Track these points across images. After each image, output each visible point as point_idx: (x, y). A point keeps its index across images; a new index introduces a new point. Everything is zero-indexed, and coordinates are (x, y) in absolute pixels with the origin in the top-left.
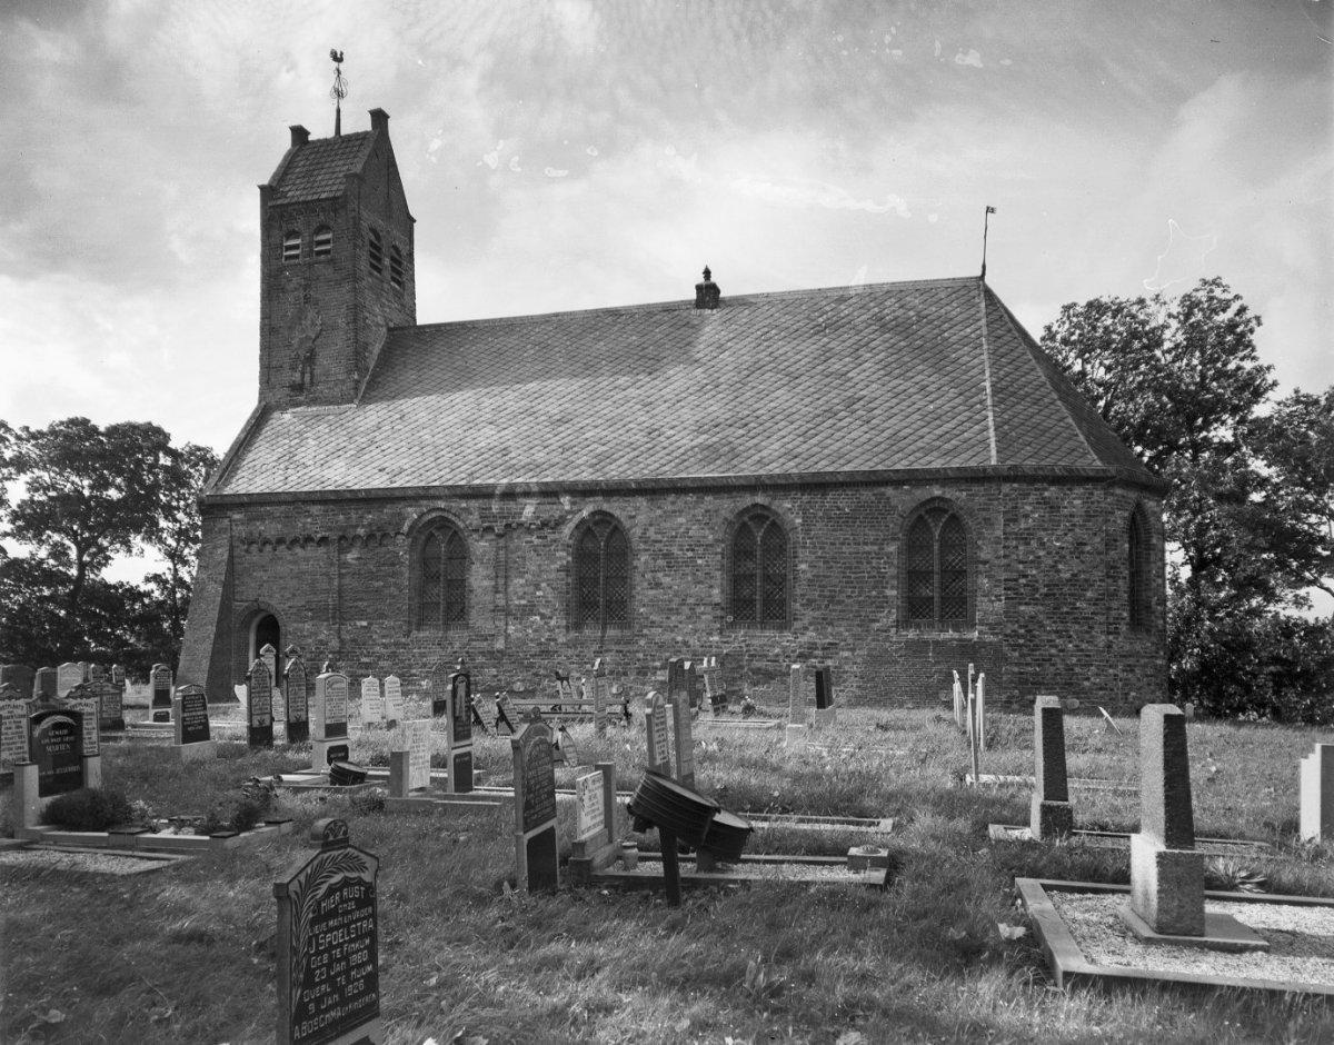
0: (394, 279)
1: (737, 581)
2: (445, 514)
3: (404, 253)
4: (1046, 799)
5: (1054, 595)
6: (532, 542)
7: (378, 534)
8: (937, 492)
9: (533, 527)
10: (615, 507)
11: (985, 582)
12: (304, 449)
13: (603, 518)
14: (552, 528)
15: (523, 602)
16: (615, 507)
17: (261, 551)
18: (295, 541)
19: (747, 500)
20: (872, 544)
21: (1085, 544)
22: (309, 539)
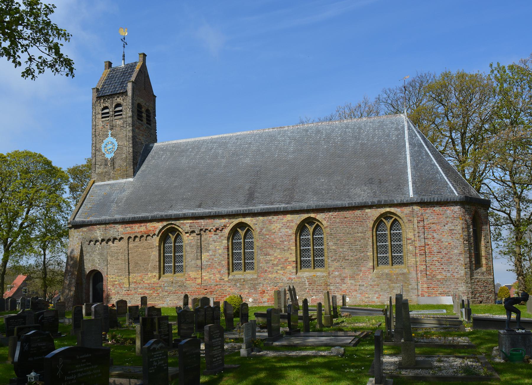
0: (147, 123)
1: (302, 253)
2: (174, 226)
3: (151, 111)
4: (240, 351)
5: (441, 252)
6: (212, 237)
7: (145, 236)
8: (388, 209)
9: (212, 230)
10: (247, 220)
11: (411, 248)
12: (260, 180)
13: (310, 221)
14: (220, 231)
15: (209, 263)
16: (247, 220)
17: (95, 244)
18: (109, 240)
19: (306, 216)
20: (361, 233)
21: (453, 230)
22: (115, 239)
